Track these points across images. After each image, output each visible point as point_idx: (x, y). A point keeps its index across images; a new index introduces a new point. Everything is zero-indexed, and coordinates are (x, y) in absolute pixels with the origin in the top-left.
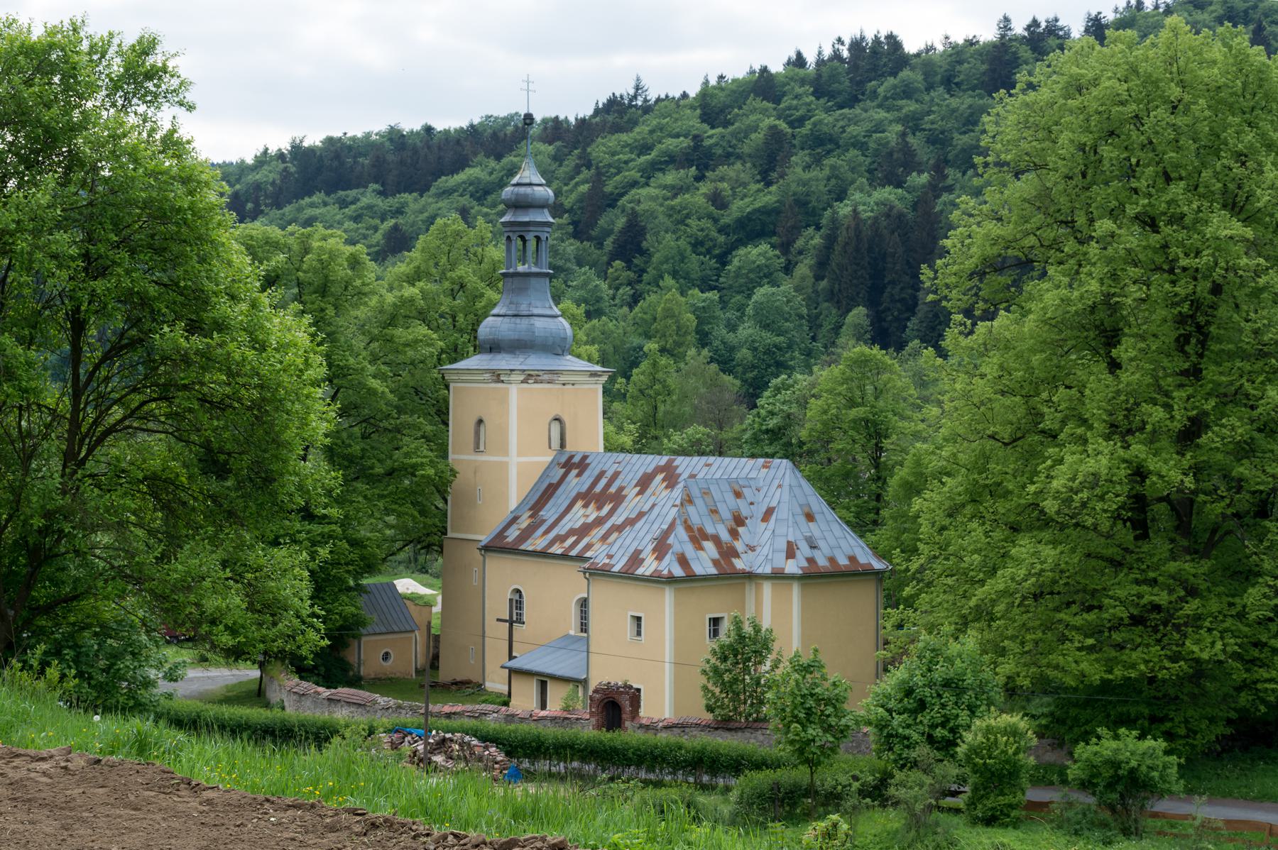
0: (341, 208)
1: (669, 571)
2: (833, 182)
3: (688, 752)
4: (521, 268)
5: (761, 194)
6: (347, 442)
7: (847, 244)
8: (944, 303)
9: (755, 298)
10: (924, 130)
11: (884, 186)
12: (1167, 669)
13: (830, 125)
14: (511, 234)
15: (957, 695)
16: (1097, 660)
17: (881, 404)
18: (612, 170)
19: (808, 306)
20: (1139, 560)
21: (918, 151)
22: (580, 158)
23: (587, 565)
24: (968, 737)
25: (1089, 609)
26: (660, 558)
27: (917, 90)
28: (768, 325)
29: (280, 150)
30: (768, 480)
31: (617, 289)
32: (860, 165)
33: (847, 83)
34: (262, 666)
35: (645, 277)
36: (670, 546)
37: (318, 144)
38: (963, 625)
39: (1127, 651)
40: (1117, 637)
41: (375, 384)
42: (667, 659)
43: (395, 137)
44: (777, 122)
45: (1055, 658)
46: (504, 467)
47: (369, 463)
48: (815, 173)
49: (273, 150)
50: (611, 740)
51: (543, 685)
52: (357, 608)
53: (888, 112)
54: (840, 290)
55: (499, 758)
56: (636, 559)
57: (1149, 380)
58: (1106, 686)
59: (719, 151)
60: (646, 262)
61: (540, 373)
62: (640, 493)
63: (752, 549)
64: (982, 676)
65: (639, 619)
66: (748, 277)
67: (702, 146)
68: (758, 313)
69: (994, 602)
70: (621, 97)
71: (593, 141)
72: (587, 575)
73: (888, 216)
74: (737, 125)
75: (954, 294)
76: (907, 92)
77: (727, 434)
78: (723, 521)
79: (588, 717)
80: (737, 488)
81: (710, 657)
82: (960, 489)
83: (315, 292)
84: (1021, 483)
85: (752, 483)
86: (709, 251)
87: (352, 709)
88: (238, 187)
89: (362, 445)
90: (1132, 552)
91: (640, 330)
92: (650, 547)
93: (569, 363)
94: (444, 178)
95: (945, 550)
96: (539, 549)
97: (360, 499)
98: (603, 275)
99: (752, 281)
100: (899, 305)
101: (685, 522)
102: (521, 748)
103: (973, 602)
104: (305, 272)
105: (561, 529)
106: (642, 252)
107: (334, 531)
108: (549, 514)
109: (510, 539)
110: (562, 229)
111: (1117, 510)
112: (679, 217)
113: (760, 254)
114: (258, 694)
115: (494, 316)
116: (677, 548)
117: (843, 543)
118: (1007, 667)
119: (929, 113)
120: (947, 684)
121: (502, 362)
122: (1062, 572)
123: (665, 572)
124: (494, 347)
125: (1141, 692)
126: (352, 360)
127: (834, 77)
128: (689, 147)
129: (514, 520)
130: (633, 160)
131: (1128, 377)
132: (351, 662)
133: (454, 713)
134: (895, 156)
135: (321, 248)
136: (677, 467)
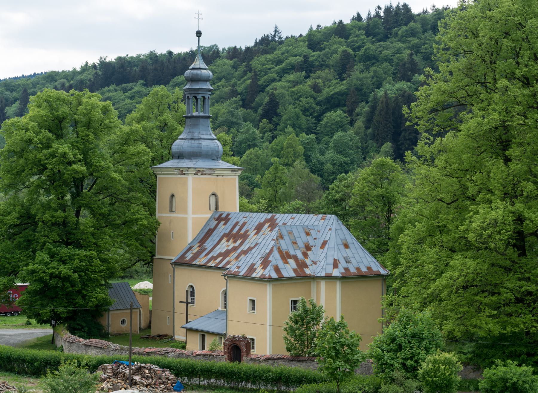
0: (124, 93)
1: (269, 275)
2: (375, 79)
3: (273, 373)
4: (195, 114)
5: (338, 85)
6: (101, 206)
7: (382, 110)
8: (416, 127)
9: (334, 137)
10: (422, 53)
11: (401, 81)
12: (535, 327)
13: (374, 50)
14: (189, 95)
15: (419, 342)
16: (498, 323)
17: (391, 188)
18: (263, 73)
19: (361, 142)
20: (520, 267)
21: (419, 64)
22: (246, 67)
23: (226, 272)
24: (424, 365)
25: (493, 294)
26: (264, 268)
27: (418, 32)
28: (341, 152)
29: (94, 63)
30: (324, 227)
31: (264, 133)
32: (389, 71)
33: (383, 29)
34: (54, 327)
35: (279, 127)
36: (270, 262)
37: (113, 60)
38: (424, 305)
39: (514, 317)
40: (508, 309)
41: (115, 175)
42: (268, 324)
43: (153, 56)
44: (347, 49)
45: (474, 321)
46: (185, 220)
47: (113, 218)
48: (366, 74)
49: (90, 63)
50: (232, 367)
51: (203, 337)
52: (105, 295)
53: (403, 43)
54: (378, 134)
55: (171, 377)
56: (252, 269)
57: (525, 168)
58: (502, 337)
59: (317, 64)
60: (279, 120)
61: (205, 170)
62: (257, 233)
63: (315, 263)
64: (433, 331)
65: (253, 301)
66: (331, 128)
67: (308, 61)
68: (336, 146)
69: (441, 291)
70: (268, 35)
71: (253, 58)
72: (226, 277)
73: (403, 96)
74: (327, 50)
75: (421, 122)
76: (413, 33)
77: (312, 205)
78: (299, 248)
79: (223, 354)
80: (307, 230)
81: (288, 321)
82: (423, 229)
83: (84, 126)
84: (456, 225)
85: (315, 227)
86: (311, 114)
87: (97, 350)
88: (72, 82)
89: (109, 208)
90: (517, 263)
91: (275, 154)
92: (260, 262)
93: (221, 164)
94: (177, 77)
95: (415, 262)
96: (202, 263)
97: (107, 237)
98: (257, 126)
99: (333, 129)
100: (408, 142)
101: (279, 248)
102: (183, 371)
103: (429, 291)
104: (78, 115)
105: (215, 253)
106: (278, 115)
107: (92, 254)
108: (209, 245)
109: (187, 259)
110: (236, 103)
111: (508, 239)
112: (296, 97)
113: (337, 116)
114: (51, 343)
115: (180, 139)
116: (274, 262)
117: (364, 260)
118: (448, 326)
119: (424, 44)
120: (414, 336)
121: (184, 164)
122: (478, 274)
123: (267, 276)
124: (180, 156)
125: (522, 340)
126: (103, 163)
127: (376, 26)
128: (302, 61)
129: (190, 248)
130: (273, 68)
131: (514, 166)
132: (103, 325)
133: (151, 353)
134: (407, 66)
135: (87, 102)
136: (277, 219)
